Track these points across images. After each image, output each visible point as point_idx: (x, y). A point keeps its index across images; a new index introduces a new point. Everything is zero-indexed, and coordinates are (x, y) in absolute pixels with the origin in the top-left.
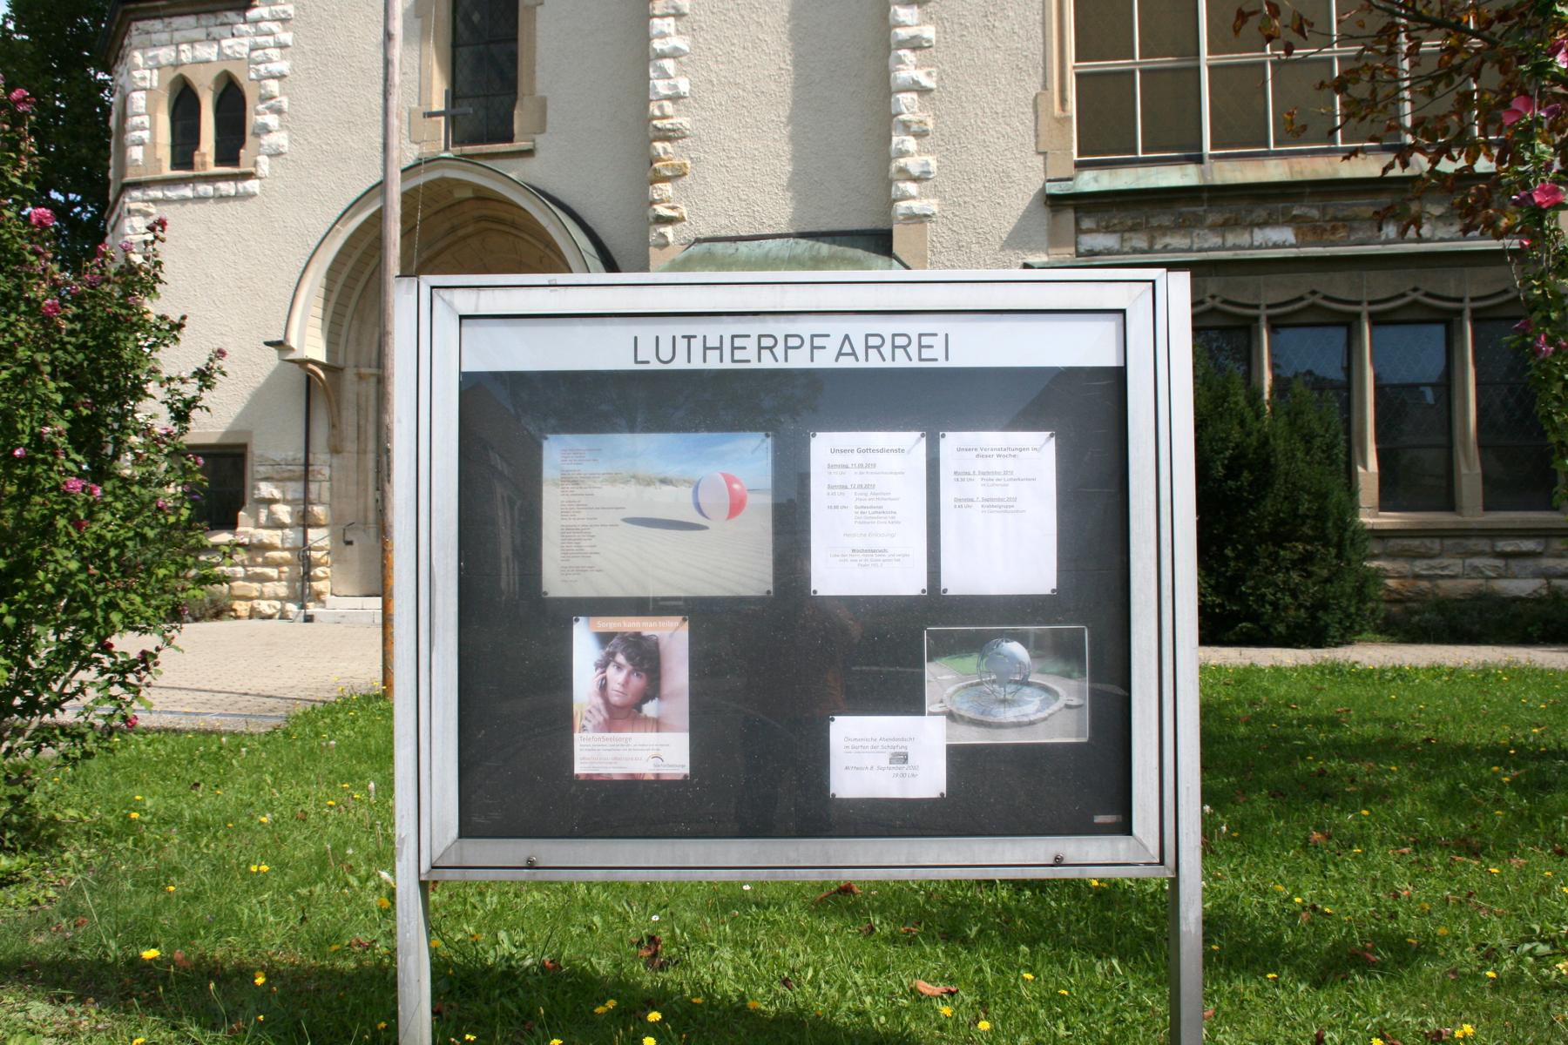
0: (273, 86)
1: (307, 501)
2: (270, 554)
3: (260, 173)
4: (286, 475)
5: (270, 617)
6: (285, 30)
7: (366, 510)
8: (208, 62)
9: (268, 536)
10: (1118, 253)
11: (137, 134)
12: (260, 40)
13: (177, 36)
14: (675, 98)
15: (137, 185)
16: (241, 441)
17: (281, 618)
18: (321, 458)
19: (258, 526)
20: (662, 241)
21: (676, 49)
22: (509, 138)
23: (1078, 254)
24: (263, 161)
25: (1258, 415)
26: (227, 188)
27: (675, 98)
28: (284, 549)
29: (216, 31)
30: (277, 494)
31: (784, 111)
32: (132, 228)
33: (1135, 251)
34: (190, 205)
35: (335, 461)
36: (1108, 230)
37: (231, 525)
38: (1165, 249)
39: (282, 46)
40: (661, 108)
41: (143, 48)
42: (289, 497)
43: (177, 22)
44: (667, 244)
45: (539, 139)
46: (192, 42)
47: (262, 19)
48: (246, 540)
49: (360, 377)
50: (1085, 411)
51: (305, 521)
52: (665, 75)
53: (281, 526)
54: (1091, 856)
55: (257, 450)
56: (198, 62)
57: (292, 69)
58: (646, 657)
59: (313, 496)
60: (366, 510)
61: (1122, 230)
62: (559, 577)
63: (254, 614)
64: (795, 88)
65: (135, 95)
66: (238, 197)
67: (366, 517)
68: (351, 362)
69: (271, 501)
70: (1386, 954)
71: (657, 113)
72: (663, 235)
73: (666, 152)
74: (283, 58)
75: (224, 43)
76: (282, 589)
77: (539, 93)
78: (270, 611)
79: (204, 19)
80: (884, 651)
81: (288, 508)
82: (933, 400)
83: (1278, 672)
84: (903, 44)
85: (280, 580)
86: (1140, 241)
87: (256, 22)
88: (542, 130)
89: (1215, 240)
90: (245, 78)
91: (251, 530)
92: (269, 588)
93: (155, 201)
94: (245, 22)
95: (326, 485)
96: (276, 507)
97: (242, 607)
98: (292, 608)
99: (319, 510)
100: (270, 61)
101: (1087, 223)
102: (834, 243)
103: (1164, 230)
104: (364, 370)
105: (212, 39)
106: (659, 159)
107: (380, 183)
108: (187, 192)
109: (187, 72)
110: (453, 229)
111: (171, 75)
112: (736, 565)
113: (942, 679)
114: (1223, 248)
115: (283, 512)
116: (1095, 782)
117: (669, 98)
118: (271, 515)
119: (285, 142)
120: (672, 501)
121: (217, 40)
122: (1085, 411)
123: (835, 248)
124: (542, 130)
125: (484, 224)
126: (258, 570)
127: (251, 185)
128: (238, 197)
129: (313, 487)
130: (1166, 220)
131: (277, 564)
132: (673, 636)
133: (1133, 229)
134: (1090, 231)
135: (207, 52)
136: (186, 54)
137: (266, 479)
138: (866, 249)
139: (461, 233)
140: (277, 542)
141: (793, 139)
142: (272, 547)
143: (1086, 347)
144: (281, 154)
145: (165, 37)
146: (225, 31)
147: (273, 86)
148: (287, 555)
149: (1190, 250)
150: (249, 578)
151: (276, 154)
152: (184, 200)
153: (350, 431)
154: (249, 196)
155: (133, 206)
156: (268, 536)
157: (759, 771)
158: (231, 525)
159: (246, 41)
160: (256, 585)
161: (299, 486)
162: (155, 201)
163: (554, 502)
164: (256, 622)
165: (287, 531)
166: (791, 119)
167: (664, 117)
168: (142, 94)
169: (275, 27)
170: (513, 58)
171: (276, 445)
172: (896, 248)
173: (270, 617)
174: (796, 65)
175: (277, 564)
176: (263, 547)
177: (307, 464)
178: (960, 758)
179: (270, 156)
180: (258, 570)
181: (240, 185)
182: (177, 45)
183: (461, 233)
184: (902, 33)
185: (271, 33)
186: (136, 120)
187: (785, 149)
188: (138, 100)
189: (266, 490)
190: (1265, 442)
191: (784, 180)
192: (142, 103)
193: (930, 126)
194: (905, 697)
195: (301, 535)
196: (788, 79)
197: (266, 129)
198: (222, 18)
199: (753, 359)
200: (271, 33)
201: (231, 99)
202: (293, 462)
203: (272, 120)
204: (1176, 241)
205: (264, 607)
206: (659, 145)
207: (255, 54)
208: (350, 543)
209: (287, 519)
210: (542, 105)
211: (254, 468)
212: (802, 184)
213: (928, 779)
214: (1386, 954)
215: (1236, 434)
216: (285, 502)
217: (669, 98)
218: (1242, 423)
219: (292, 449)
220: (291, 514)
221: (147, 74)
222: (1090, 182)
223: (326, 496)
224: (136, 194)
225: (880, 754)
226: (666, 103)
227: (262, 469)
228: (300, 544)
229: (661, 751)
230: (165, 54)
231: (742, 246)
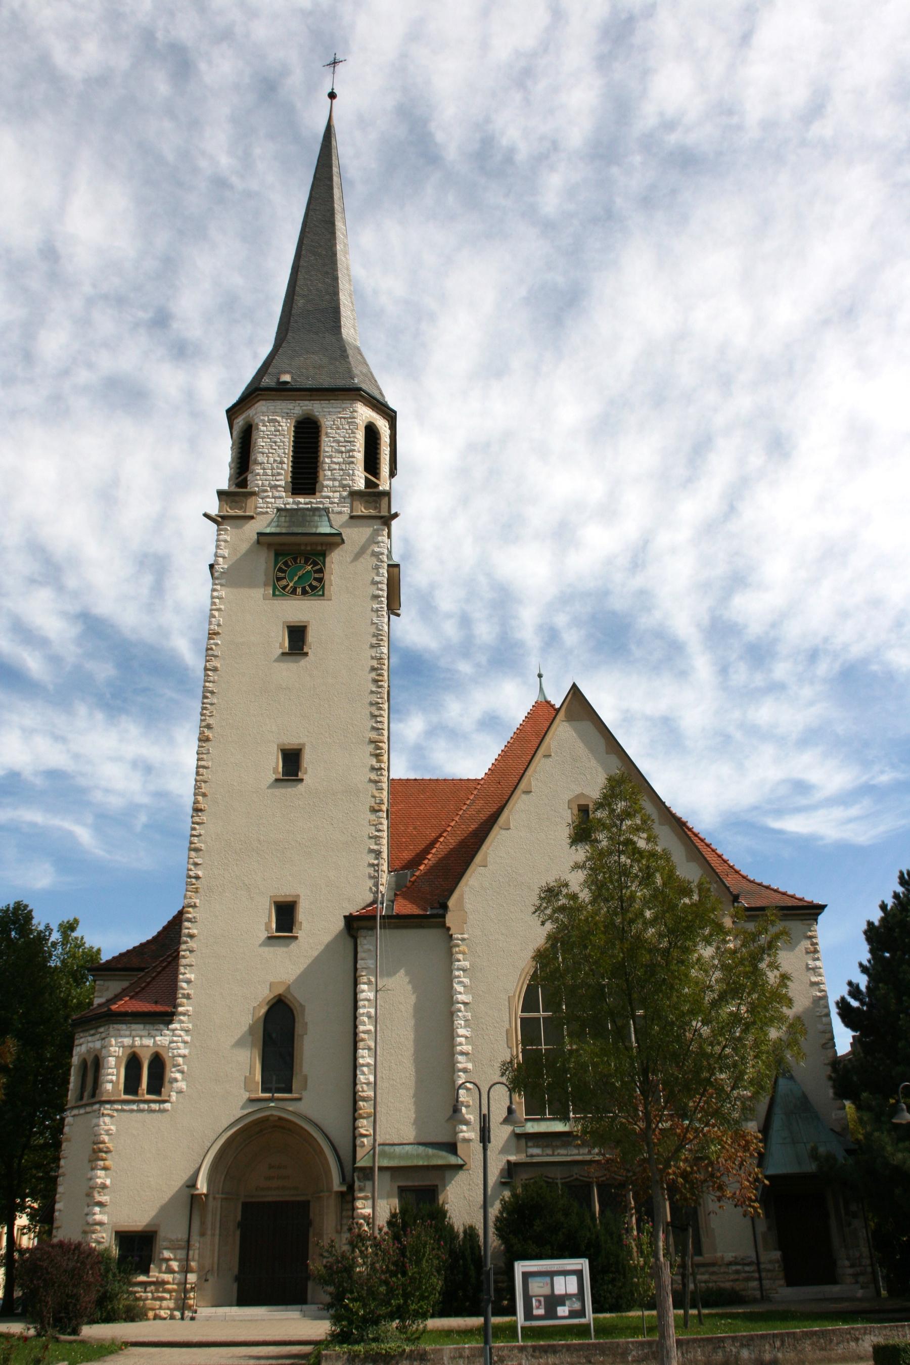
0: (180, 1060)
1: (187, 1260)
5: (165, 1319)
6: (187, 1035)
8: (148, 1046)
9: (168, 1277)
10: (541, 1156)
11: (110, 1077)
12: (175, 1039)
13: (134, 1033)
15: (108, 1102)
16: (154, 1229)
19: (160, 1272)
22: (290, 1091)
23: (527, 1156)
24: (173, 1094)
25: (595, 1225)
26: (155, 1106)
28: (173, 1284)
29: (154, 1033)
30: (172, 1256)
31: (412, 1092)
32: (104, 1122)
33: (547, 1155)
34: (135, 1114)
36: (538, 1146)
37: (146, 1272)
38: (558, 1155)
39: (185, 1042)
41: (116, 1037)
42: (178, 1257)
43: (134, 1026)
44: (364, 1146)
45: (304, 1093)
46: (141, 1037)
47: (177, 1029)
48: (154, 1279)
49: (214, 1198)
50: (579, 1273)
51: (186, 1270)
52: (363, 1073)
54: (583, 1321)
55: (162, 1234)
56: (142, 1046)
57: (190, 1053)
58: (540, 1301)
59: (191, 1257)
61: (543, 1147)
62: (531, 1293)
63: (156, 1317)
64: (416, 1082)
65: (110, 1058)
66: (160, 1111)
69: (169, 1260)
72: (363, 1142)
74: (185, 1048)
75: (158, 1038)
76: (171, 1304)
78: (165, 1316)
79: (148, 1027)
80: (561, 1300)
82: (565, 1273)
83: (605, 1318)
84: (460, 1070)
85: (170, 1299)
86: (549, 1151)
87: (174, 1030)
88: (305, 1089)
89: (575, 1151)
90: (167, 1056)
91: (157, 1274)
92: (165, 1304)
93: (117, 1110)
94: (168, 1030)
95: (197, 1252)
97: (151, 1314)
98: (177, 1314)
99: (193, 1264)
100: (179, 1048)
101: (530, 1144)
102: (436, 1149)
103: (557, 1147)
104: (217, 1196)
105: (150, 1036)
106: (361, 1109)
108: (135, 1107)
109: (138, 1050)
111: (129, 1051)
112: (546, 1291)
113: (567, 1303)
114: (579, 1154)
115: (175, 1265)
116: (581, 1313)
119: (185, 1087)
120: (541, 1285)
121: (154, 1037)
122: (579, 1273)
123: (435, 1151)
124: (305, 1089)
126: (160, 1295)
127: (167, 1106)
128: (160, 1111)
129: (191, 1253)
130: (558, 1143)
131: (169, 1291)
132: (542, 1299)
133: (547, 1146)
134: (531, 1147)
135: (149, 1042)
136: (138, 1042)
137: (166, 1248)
138: (447, 1151)
140: (171, 1280)
141: (415, 1103)
142: (168, 1283)
143: (579, 1267)
145: (128, 1033)
146: (158, 1033)
147: (180, 1060)
148: (175, 1287)
149: (567, 1155)
150: (154, 1299)
151: (180, 1092)
152: (132, 1111)
154: (165, 1111)
155: (106, 1112)
156: (168, 1277)
157: (551, 1313)
158: (146, 1272)
159: (168, 1038)
160: (158, 1303)
162: (117, 1110)
163: (530, 1285)
164: (158, 1322)
166: (415, 1095)
167: (363, 1091)
168: (114, 1059)
169: (182, 1033)
170: (291, 1055)
171: (172, 1231)
172: (459, 1152)
173: (165, 1319)
174: (416, 1072)
175: (169, 1291)
176: (164, 1283)
178: (570, 1311)
179: (177, 1093)
180: (160, 1295)
181: (162, 1106)
182: (134, 1037)
184: (460, 1066)
185: (180, 1036)
186: (110, 1071)
187: (412, 1108)
188: (112, 1061)
189: (167, 1254)
190: (597, 1237)
191: (412, 1121)
192: (113, 1063)
193: (471, 1103)
194: (564, 1304)
195: (183, 1277)
196: (413, 1079)
197: (176, 1080)
198: (157, 1027)
199: (549, 1269)
200: (180, 1036)
201: (158, 1064)
203: (178, 1076)
204: (562, 1151)
205: (163, 1313)
207: (172, 1045)
208: (206, 1280)
209: (176, 1269)
210: (305, 1078)
211: (160, 1242)
212: (419, 1122)
213: (567, 1313)
215: (588, 1234)
216: (175, 1259)
218: (590, 1230)
219: (181, 1234)
220: (179, 1266)
221: (117, 1049)
222: (532, 1128)
223: (196, 1257)
224: (108, 1106)
225: (562, 1311)
227: (164, 1243)
228: (183, 1281)
229: (541, 1312)
230: (127, 1041)
231: (396, 1148)
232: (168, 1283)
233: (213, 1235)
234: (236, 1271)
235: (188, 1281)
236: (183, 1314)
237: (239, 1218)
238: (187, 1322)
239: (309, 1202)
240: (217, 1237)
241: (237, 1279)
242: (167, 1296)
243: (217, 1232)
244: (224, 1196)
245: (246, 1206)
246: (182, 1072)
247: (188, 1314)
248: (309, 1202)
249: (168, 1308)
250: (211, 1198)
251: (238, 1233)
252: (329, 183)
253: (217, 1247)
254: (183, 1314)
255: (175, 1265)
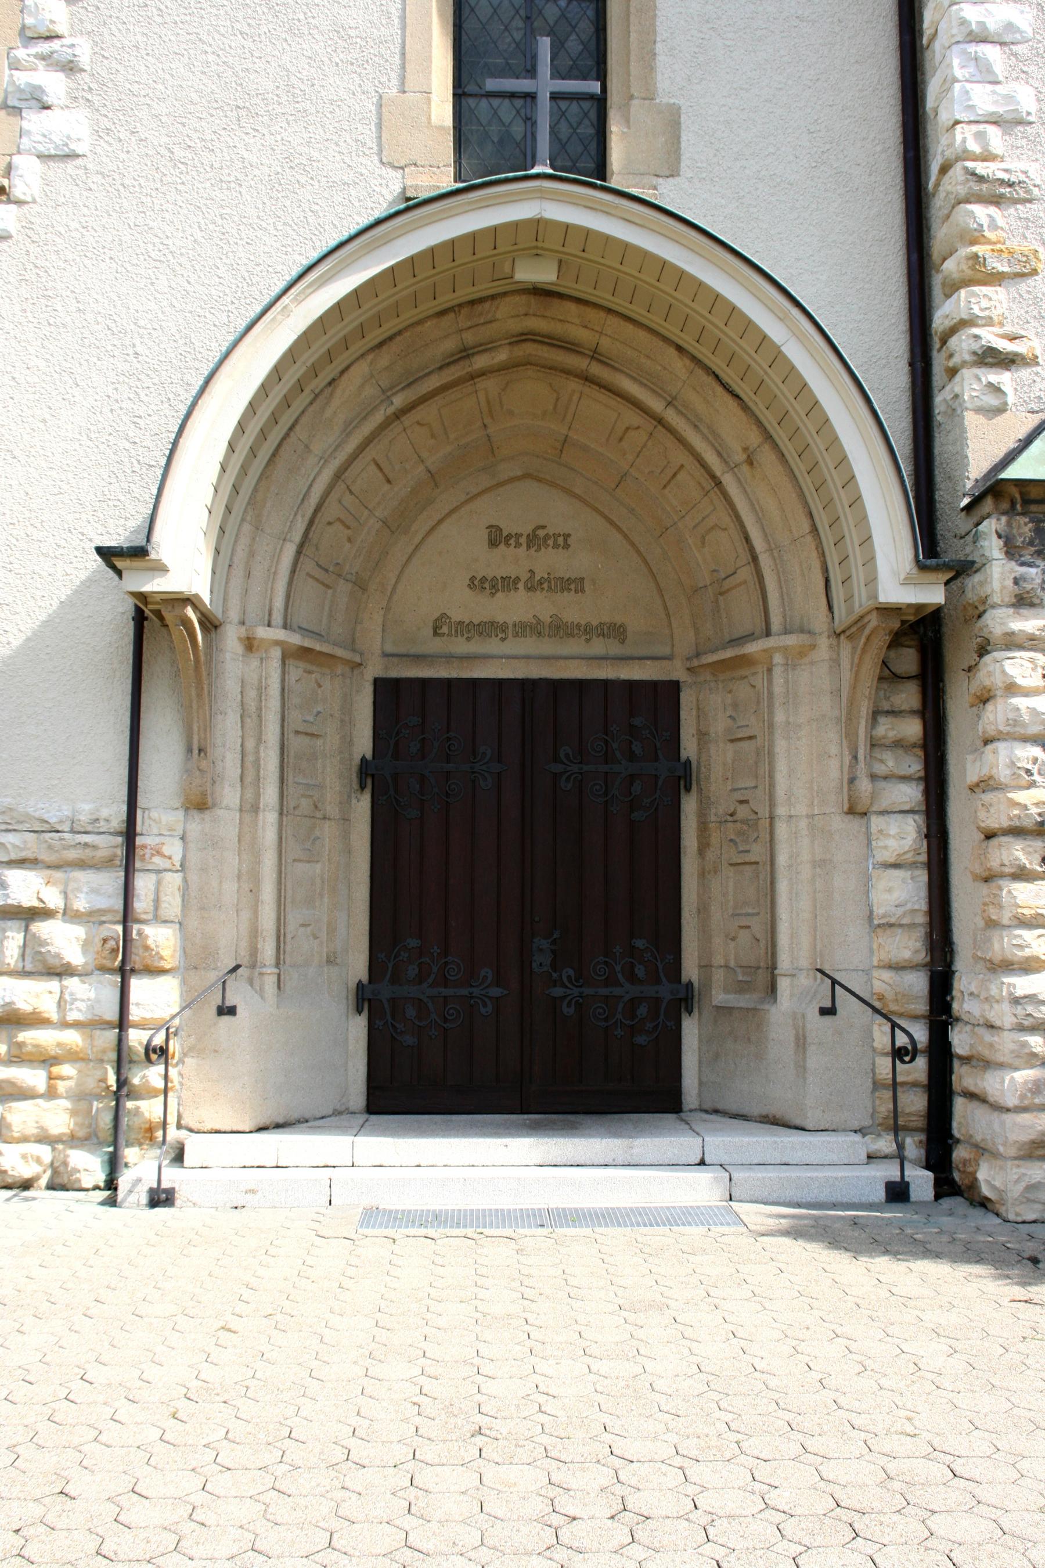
2: (28, 1036)
3: (18, 191)
4: (72, 855)
5: (26, 1185)
7: (255, 933)
14: (1009, 122)
17: (51, 1187)
18: (162, 823)
20: (993, 401)
21: (1010, 27)
27: (1009, 122)
28: (65, 1025)
30: (53, 899)
35: (196, 826)
40: (980, 136)
42: (81, 904)
49: (250, 644)
53: (60, 971)
59: (141, 904)
60: (255, 933)
67: (254, 952)
68: (234, 615)
69: (31, 915)
70: (34, 1199)
71: (974, 147)
72: (996, 389)
73: (994, 226)
76: (58, 1117)
77: (662, 99)
78: (26, 1171)
81: (79, 931)
85: (51, 1094)
95: (173, 881)
96: (42, 928)
99: (161, 939)
104: (262, 633)
107: (601, 170)
110: (465, 353)
117: (996, 121)
118: (31, 945)
125: (529, 349)
129: (143, 884)
131: (47, 1060)
137: (21, 863)
139: (480, 362)
140: (49, 1008)
142: (36, 1020)
144: (73, 156)
148: (73, 1038)
153: (229, 762)
161: (111, 881)
165: (73, 983)
167: (987, 157)
173: (26, 1185)
175: (47, 1060)
177: (130, 833)
183: (480, 362)
202: (93, 827)
206: (981, 212)
208: (227, 1011)
209: (75, 957)
214: (34, 1199)
216: (70, 915)
217: (996, 121)
220: (86, 945)
223: (172, 904)
226: (992, 131)
228: (111, 1013)
232: (36, 1020)
233: (251, 808)
234: (358, 966)
235: (135, 1013)
236: (114, 1164)
237: (363, 744)
238: (133, 1214)
239: (674, 688)
240: (269, 818)
241: (365, 998)
242: (34, 1078)
243: (270, 794)
244: (295, 639)
245: (390, 694)
246: (70, 68)
247: (141, 1167)
248: (674, 688)
249: (44, 1138)
250: (231, 638)
251: (362, 806)
252: (379, 1023)
253: (269, 860)
254: (114, 1164)
255: (65, 940)
